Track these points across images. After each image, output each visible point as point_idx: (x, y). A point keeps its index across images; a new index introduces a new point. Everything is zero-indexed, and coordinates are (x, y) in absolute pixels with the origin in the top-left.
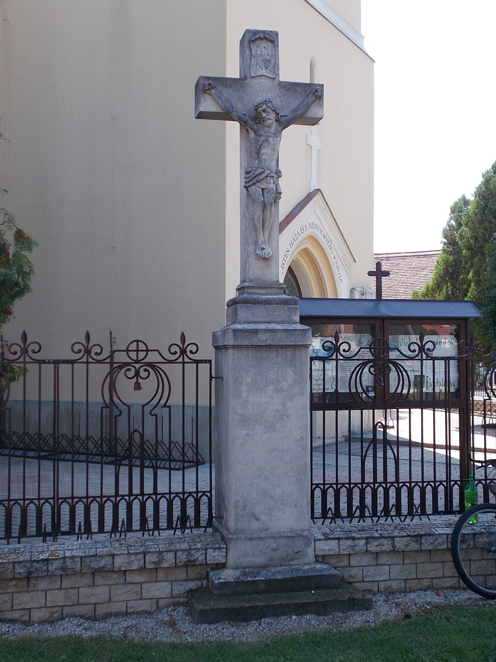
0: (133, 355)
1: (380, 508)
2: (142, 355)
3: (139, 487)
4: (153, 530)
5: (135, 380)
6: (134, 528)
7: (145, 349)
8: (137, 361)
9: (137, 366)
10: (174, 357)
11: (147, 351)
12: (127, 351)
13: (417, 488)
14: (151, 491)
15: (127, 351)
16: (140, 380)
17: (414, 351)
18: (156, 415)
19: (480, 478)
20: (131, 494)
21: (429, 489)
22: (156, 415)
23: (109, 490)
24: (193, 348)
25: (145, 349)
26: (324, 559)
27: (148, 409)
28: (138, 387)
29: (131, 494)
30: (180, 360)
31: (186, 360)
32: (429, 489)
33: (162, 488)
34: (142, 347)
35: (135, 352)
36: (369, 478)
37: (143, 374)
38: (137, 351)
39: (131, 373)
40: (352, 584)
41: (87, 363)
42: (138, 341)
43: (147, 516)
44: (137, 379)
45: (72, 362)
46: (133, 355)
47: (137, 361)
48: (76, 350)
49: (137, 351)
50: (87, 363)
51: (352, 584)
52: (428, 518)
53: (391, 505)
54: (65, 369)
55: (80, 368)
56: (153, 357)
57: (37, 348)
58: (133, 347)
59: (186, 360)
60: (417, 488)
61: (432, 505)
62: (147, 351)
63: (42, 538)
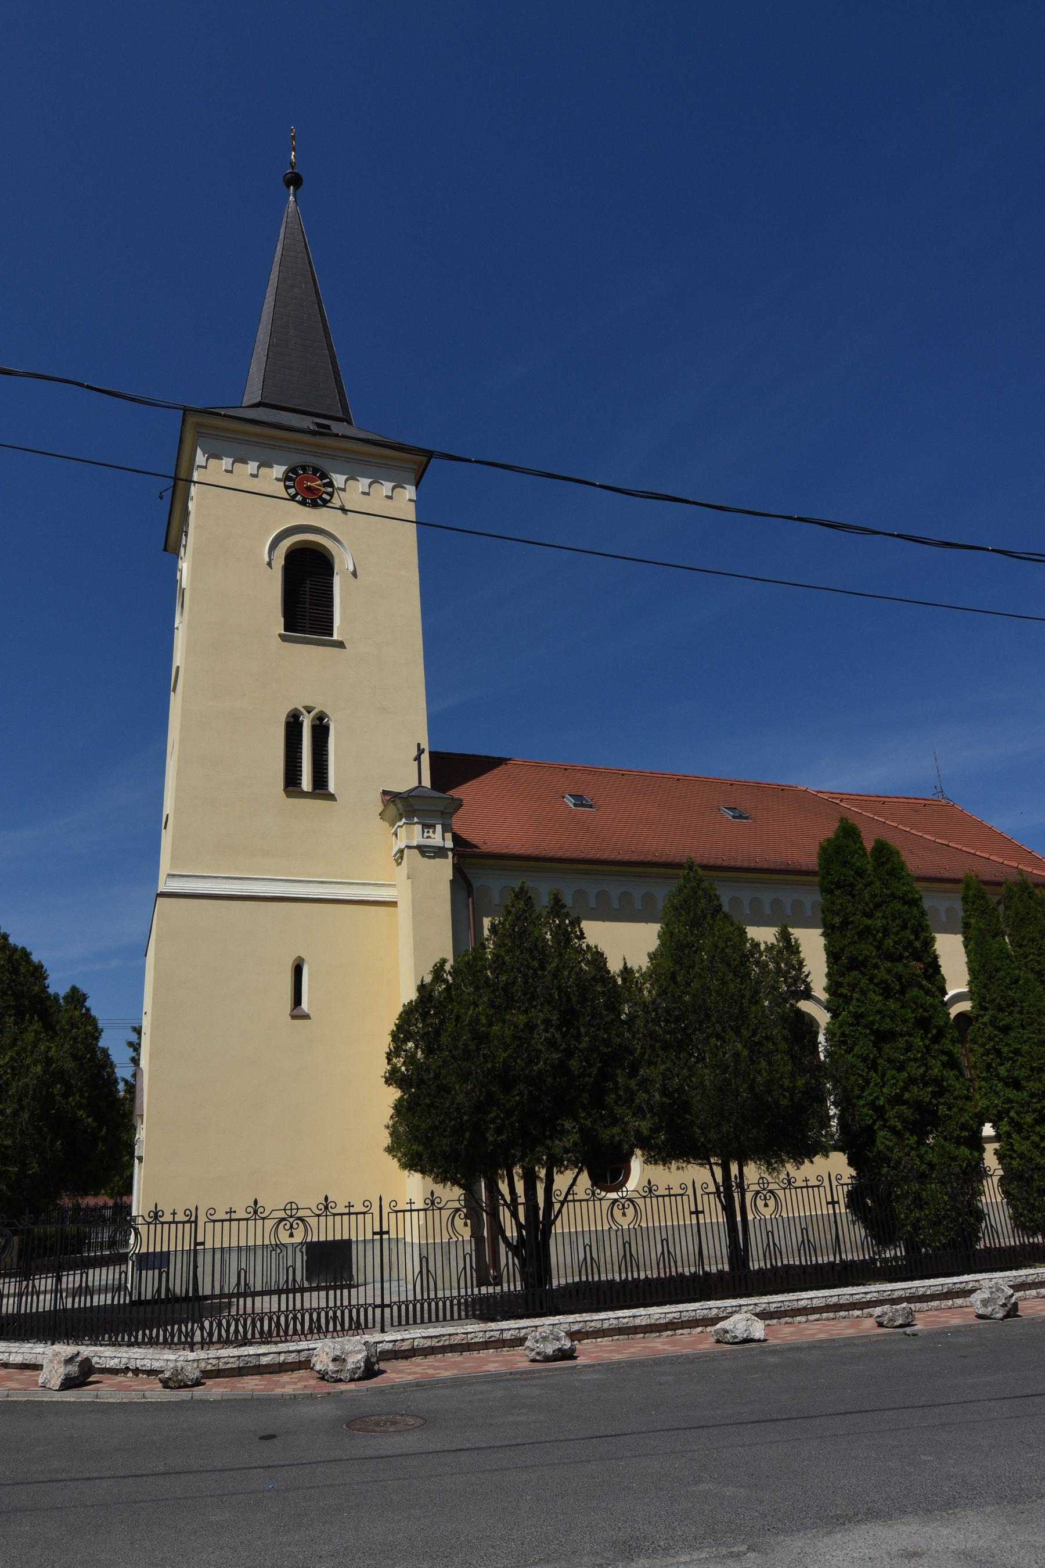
0: (289, 1212)
1: (306, 1327)
2: (294, 1212)
3: (348, 1300)
4: (333, 1332)
6: (369, 1327)
8: (623, 1198)
9: (291, 1220)
10: (321, 1212)
11: (298, 1209)
13: (266, 1317)
14: (434, 1297)
15: (285, 1210)
17: (321, 1210)
19: (370, 1303)
20: (328, 1306)
21: (362, 1310)
23: (323, 1304)
24: (333, 1205)
26: (786, 1314)
29: (328, 1306)
30: (324, 1214)
31: (435, 1208)
32: (362, 1310)
33: (307, 1305)
34: (294, 1206)
36: (419, 1297)
37: (295, 1226)
38: (291, 1209)
41: (255, 1219)
42: (291, 1203)
45: (247, 1220)
46: (289, 1212)
48: (366, 1205)
49: (291, 1209)
50: (255, 1219)
54: (679, 1198)
55: (251, 1223)
56: (300, 1214)
57: (333, 1206)
58: (289, 1207)
59: (435, 1208)
60: (411, 1304)
62: (298, 1209)
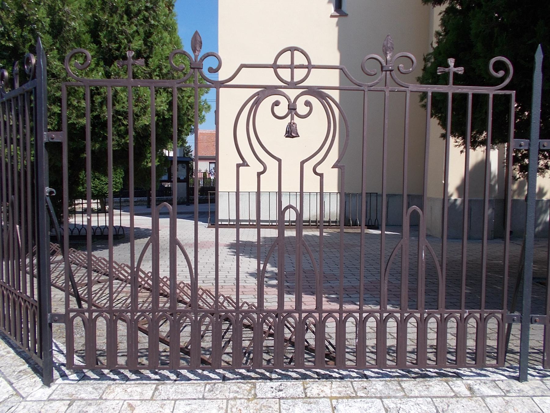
0: (285, 74)
5: (288, 120)
7: (306, 63)
9: (292, 93)
12: (275, 66)
15: (275, 66)
16: (296, 120)
18: (321, 175)
22: (321, 175)
25: (306, 63)
27: (309, 167)
28: (291, 133)
35: (289, 63)
37: (302, 109)
39: (282, 110)
40: (26, 165)
42: (292, 49)
43: (190, 338)
44: (292, 118)
47: (293, 85)
51: (26, 165)
52: (533, 400)
53: (472, 369)
58: (285, 59)
61: (141, 265)
62: (309, 67)
63: (96, 234)
